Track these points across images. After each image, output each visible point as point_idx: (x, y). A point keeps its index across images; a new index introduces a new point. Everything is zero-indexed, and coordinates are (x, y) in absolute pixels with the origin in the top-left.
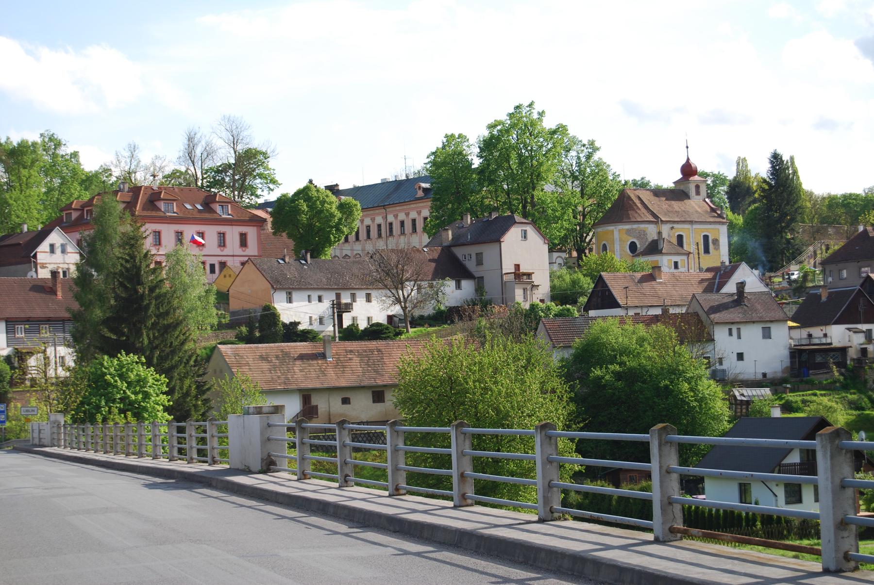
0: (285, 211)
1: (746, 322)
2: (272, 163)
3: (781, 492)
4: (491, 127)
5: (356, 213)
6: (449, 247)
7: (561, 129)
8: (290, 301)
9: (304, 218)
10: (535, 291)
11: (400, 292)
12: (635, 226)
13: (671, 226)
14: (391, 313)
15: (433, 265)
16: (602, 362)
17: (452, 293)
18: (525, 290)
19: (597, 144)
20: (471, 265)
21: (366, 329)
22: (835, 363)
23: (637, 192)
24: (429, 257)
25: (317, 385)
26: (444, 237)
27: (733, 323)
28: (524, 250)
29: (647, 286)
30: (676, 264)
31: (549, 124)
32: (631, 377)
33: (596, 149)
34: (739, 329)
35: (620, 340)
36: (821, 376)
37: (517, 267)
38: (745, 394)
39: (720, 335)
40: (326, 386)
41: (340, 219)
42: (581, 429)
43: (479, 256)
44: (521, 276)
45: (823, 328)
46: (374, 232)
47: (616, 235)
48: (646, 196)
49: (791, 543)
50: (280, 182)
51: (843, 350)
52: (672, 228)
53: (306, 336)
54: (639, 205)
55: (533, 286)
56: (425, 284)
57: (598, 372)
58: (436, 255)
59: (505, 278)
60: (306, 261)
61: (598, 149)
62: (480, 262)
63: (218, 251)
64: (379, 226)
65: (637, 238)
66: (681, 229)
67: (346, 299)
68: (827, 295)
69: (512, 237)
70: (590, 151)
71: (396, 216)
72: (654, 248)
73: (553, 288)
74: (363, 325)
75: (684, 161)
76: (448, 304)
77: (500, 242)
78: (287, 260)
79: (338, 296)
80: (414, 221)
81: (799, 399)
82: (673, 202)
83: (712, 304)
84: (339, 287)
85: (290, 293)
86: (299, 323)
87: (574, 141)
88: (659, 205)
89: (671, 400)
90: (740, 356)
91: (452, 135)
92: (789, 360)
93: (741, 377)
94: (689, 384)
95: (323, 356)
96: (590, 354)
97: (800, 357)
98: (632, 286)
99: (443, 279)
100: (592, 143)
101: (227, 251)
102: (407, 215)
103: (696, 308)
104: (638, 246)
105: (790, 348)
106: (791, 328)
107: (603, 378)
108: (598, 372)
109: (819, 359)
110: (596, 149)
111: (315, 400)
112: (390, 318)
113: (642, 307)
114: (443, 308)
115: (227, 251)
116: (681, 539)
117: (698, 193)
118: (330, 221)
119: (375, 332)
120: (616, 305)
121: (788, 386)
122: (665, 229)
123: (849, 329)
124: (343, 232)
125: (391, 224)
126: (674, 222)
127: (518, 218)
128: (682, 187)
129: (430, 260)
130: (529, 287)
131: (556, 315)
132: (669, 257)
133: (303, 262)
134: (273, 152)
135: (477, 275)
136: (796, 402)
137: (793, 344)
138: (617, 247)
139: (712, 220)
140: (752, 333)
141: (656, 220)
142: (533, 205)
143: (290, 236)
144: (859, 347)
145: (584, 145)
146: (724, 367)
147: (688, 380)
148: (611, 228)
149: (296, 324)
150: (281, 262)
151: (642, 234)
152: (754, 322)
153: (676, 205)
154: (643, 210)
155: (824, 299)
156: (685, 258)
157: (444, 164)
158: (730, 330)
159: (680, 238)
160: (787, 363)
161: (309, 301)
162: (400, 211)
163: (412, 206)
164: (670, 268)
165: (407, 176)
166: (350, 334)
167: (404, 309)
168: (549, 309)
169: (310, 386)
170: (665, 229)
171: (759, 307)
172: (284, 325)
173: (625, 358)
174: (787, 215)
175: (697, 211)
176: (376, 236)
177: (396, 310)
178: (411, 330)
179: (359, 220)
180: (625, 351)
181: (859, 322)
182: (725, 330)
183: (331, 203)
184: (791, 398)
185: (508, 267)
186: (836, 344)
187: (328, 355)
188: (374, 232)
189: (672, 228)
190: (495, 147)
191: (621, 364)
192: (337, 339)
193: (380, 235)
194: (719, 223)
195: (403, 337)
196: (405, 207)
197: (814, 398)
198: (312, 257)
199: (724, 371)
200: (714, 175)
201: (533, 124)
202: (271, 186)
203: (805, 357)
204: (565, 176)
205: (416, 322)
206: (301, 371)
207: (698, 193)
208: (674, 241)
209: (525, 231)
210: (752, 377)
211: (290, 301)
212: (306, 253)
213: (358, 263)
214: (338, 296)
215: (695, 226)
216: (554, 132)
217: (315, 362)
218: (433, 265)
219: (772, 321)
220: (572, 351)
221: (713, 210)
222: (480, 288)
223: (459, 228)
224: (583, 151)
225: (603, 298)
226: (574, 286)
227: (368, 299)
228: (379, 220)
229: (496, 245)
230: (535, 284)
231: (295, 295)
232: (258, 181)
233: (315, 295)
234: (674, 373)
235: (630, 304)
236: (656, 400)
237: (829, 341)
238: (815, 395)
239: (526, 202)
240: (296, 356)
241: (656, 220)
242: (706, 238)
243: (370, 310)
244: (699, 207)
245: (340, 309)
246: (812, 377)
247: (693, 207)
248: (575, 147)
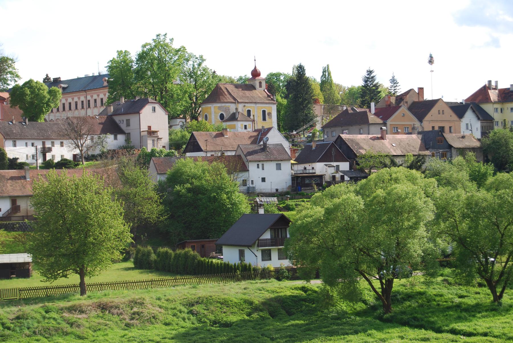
0: (17, 94)
1: (267, 161)
2: (16, 65)
3: (259, 254)
4: (144, 46)
5: (58, 96)
6: (111, 115)
7: (182, 49)
8: (15, 145)
9: (28, 98)
10: (160, 142)
11: (79, 141)
12: (223, 105)
13: (244, 105)
14: (75, 153)
15: (101, 126)
16: (182, 183)
17: (111, 142)
18: (153, 141)
19: (204, 58)
20: (123, 126)
21: (58, 162)
22: (315, 184)
23: (225, 86)
24: (99, 121)
25: (20, 194)
26: (108, 110)
27: (259, 161)
28: (153, 118)
29: (219, 140)
30: (246, 127)
31: (176, 46)
32: (196, 191)
33: (203, 60)
34: (263, 165)
35: (193, 170)
36: (308, 191)
37: (150, 127)
38: (263, 200)
39: (252, 167)
40: (25, 194)
41: (49, 99)
43: (128, 121)
44: (151, 133)
45: (311, 164)
46: (79, 106)
47: (213, 110)
48: (231, 88)
50: (21, 77)
51: (321, 177)
52: (244, 106)
53: (21, 166)
54: (226, 93)
55: (158, 138)
56: (96, 137)
57: (178, 188)
58: (103, 121)
59: (142, 134)
60: (25, 123)
61: (205, 60)
62: (128, 125)
64: (82, 102)
65: (224, 111)
66: (249, 107)
67: (48, 145)
68: (315, 146)
69: (147, 110)
70: (201, 61)
71: (92, 97)
72: (233, 118)
73: (171, 140)
74: (57, 159)
75: (253, 68)
76: (109, 148)
77: (139, 114)
78: (14, 122)
79: (44, 143)
80: (70, 104)
81: (294, 203)
82: (246, 91)
83: (249, 150)
84: (44, 138)
85: (15, 141)
86: (18, 158)
87: (191, 56)
88: (237, 93)
89: (217, 204)
90: (263, 180)
91: (121, 51)
92: (291, 182)
93: (264, 191)
94: (227, 195)
95: (24, 178)
96: (176, 178)
97: (297, 180)
98: (210, 139)
99: (106, 134)
100: (201, 57)
102: (98, 96)
103: (239, 152)
104: (225, 116)
105: (292, 175)
106: (292, 164)
107: (180, 191)
108: (178, 188)
109: (307, 181)
110: (203, 60)
111: (19, 202)
112: (75, 156)
113: (215, 151)
114: (105, 150)
117: (260, 86)
118: (43, 100)
119: (64, 164)
120: (201, 150)
121: (289, 196)
122: (240, 107)
123: (326, 165)
124: (50, 107)
125: (89, 101)
126: (246, 103)
127: (150, 100)
128: (252, 83)
129: (100, 124)
130: (156, 139)
131: (165, 156)
132: (242, 123)
133: (24, 124)
134: (17, 59)
135: (126, 132)
136: (292, 205)
137: (293, 173)
138: (213, 116)
139: (267, 102)
140: (270, 167)
141: (235, 101)
142: (167, 91)
143: (21, 108)
144: (331, 175)
145: (197, 58)
146: (254, 186)
147: (227, 193)
148: (209, 105)
149: (16, 159)
150: (11, 123)
151: (227, 110)
152: (271, 161)
153: (247, 93)
154: (228, 96)
155: (314, 148)
156: (251, 123)
157: (116, 67)
158: (258, 165)
159: (249, 112)
160: (290, 183)
161: (26, 146)
162: (75, 96)
163: (101, 91)
164: (242, 129)
165: (99, 73)
166: (48, 165)
167: (81, 151)
168: (162, 152)
169: (16, 195)
170: (240, 107)
171: (275, 152)
172: (9, 160)
173: (194, 180)
174: (306, 100)
175: (259, 97)
176: (81, 107)
177: (77, 151)
178: (85, 163)
179: (61, 99)
180: (194, 177)
181: (332, 162)
182: (255, 164)
183: (43, 90)
184: (289, 203)
185: (144, 127)
186: (318, 172)
187: (27, 177)
188: (79, 106)
189: (244, 106)
190: (145, 58)
191: (192, 184)
192: (38, 168)
193: (83, 108)
194: (272, 103)
195: (80, 166)
196: (78, 94)
197: (303, 203)
198: (29, 121)
199: (254, 188)
200: (284, 75)
201: (167, 45)
202: (16, 79)
203: (299, 180)
204: (186, 76)
205: (88, 158)
206: (11, 186)
207: (260, 86)
208: (246, 114)
209: (154, 108)
210: (269, 191)
211: (15, 145)
212: (26, 118)
213: (56, 124)
214: (44, 143)
215: (258, 105)
216: (179, 50)
217: (20, 181)
218: (101, 126)
219: (282, 160)
220: (166, 176)
221: (268, 96)
222: (128, 140)
223: (118, 105)
224: (196, 61)
225: (193, 146)
226: (182, 139)
227: (62, 144)
228: (82, 98)
229: (138, 115)
230: (160, 137)
231: (18, 142)
232: (9, 75)
233: (30, 142)
234: (220, 189)
235: (208, 149)
236: (208, 204)
237: (314, 171)
238: (303, 201)
239: (163, 90)
240: (9, 177)
241: (235, 101)
242: (264, 112)
243: (61, 151)
244: (261, 94)
245: (45, 151)
246: (303, 191)
247: (257, 94)
248: (192, 59)
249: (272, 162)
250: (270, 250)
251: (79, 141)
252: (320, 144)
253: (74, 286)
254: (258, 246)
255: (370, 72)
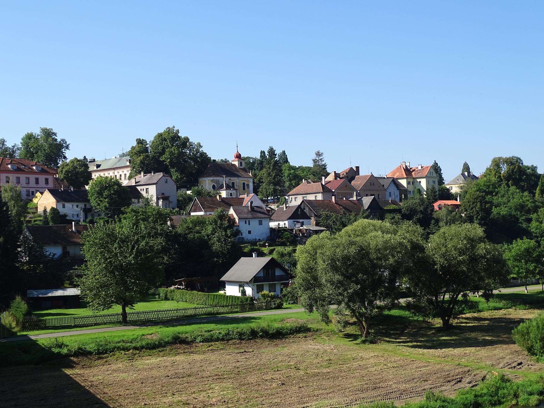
30: (231, 194)
34: (249, 221)
42: (522, 321)
49: (59, 293)
62: (147, 192)
63: (26, 186)
90: (250, 232)
101: (30, 186)
115: (30, 186)
116: (103, 310)
160: (269, 234)
242: (244, 184)
250: (263, 285)
253: (117, 314)
254: (254, 282)
255: (318, 154)
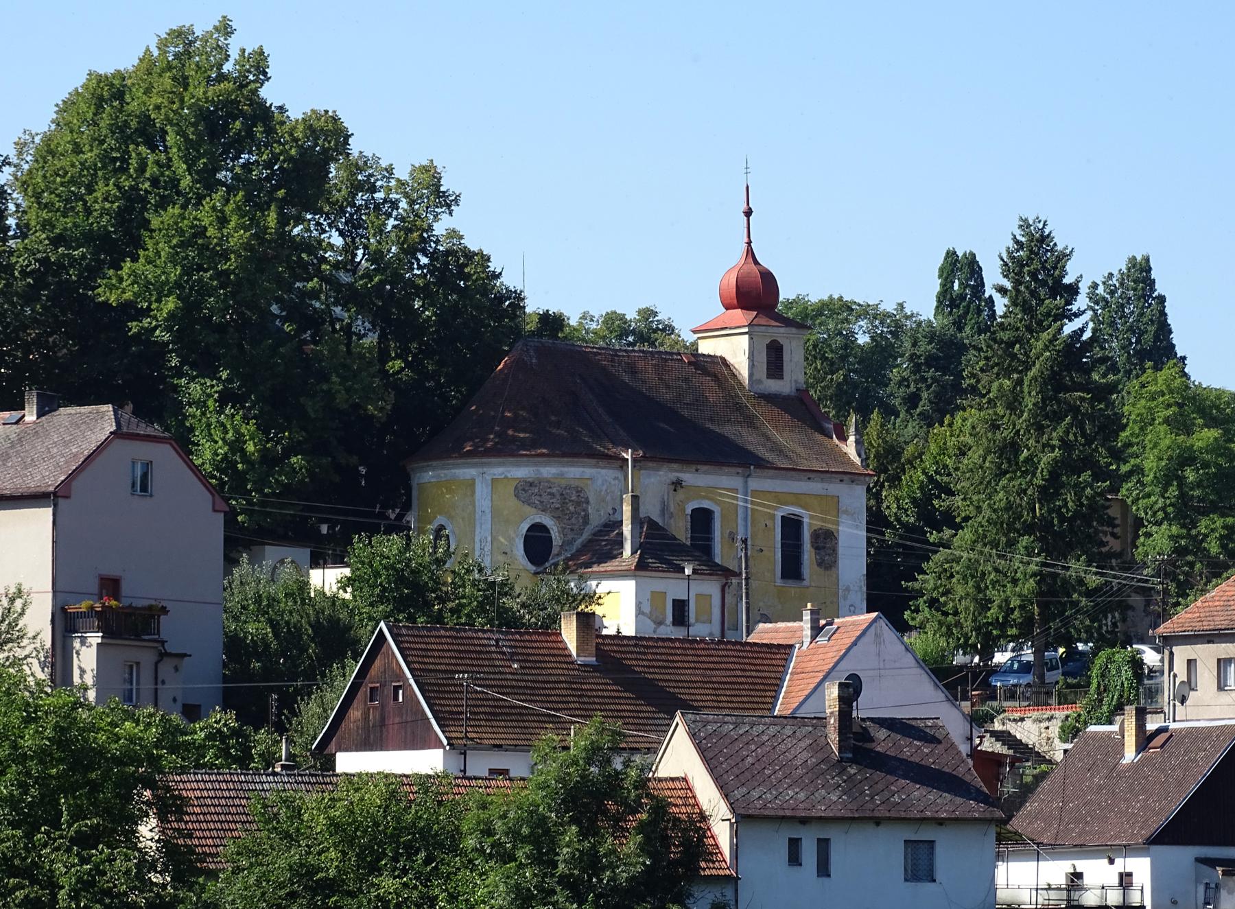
27: (804, 821)
34: (824, 846)
47: (483, 497)
85: (465, 754)
152: (878, 821)
158: (794, 844)
159: (702, 519)
219: (940, 822)
230: (170, 648)
242: (792, 526)
249: (883, 831)
251: (190, 810)
252: (423, 710)
